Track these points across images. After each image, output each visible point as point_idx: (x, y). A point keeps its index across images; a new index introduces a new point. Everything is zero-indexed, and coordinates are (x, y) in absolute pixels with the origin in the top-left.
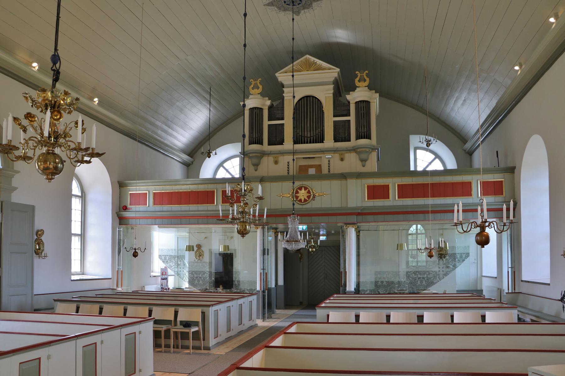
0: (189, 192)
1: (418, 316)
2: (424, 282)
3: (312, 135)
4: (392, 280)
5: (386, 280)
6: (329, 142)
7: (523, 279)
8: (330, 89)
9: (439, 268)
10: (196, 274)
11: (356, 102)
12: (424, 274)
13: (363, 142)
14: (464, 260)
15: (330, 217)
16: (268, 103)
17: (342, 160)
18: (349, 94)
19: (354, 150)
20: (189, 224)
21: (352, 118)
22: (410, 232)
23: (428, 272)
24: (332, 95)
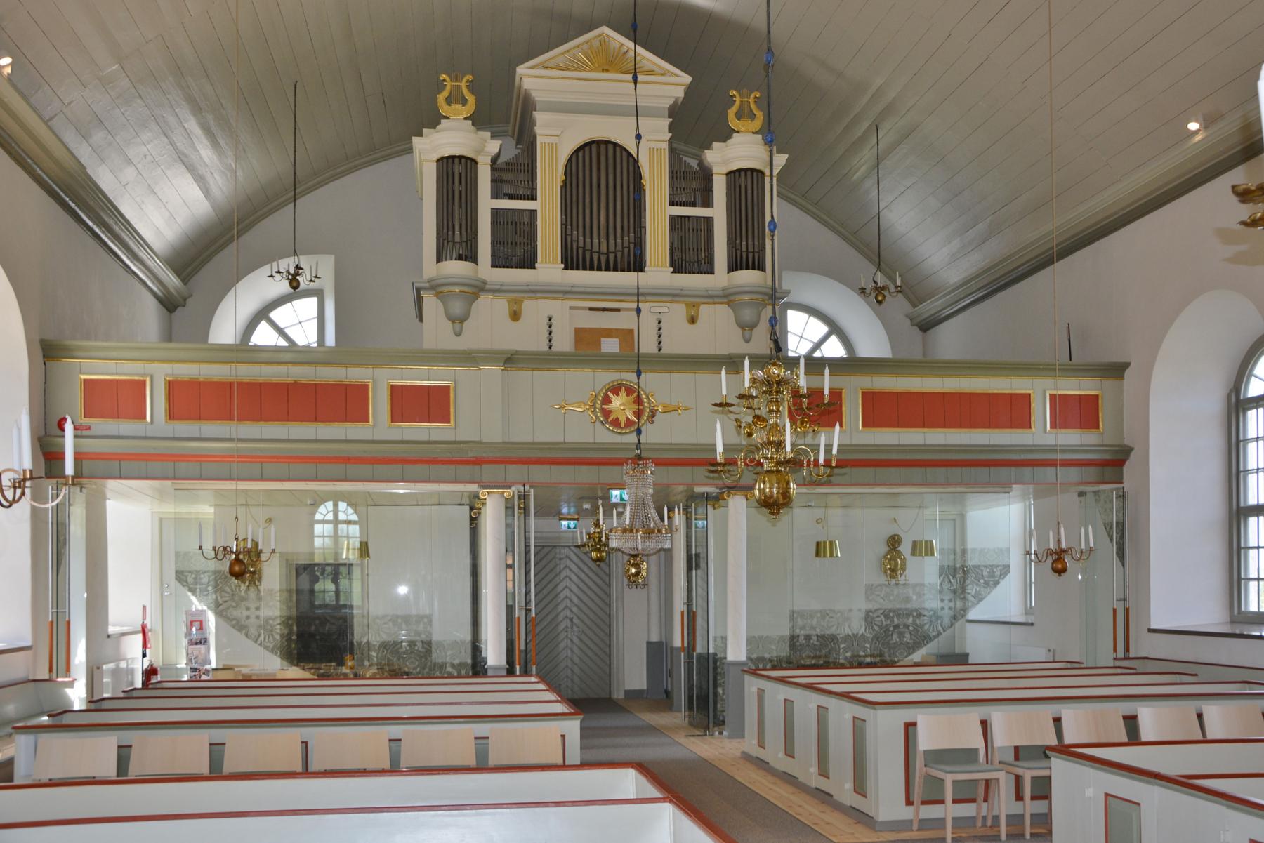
0: (288, 384)
1: (1125, 718)
2: (908, 636)
3: (612, 248)
4: (833, 631)
5: (818, 631)
6: (658, 272)
7: (1153, 627)
8: (657, 134)
9: (942, 600)
10: (898, 616)
11: (729, 174)
12: (908, 616)
13: (747, 277)
14: (997, 583)
15: (602, 468)
16: (494, 146)
17: (693, 320)
18: (420, 134)
19: (727, 297)
20: (121, 478)
21: (718, 212)
22: (318, 517)
23: (916, 610)
24: (665, 145)
